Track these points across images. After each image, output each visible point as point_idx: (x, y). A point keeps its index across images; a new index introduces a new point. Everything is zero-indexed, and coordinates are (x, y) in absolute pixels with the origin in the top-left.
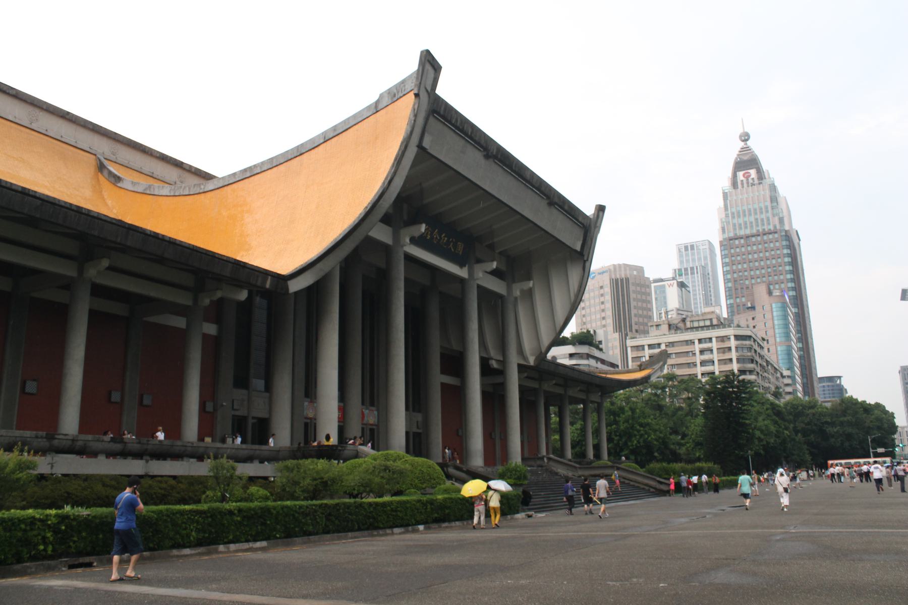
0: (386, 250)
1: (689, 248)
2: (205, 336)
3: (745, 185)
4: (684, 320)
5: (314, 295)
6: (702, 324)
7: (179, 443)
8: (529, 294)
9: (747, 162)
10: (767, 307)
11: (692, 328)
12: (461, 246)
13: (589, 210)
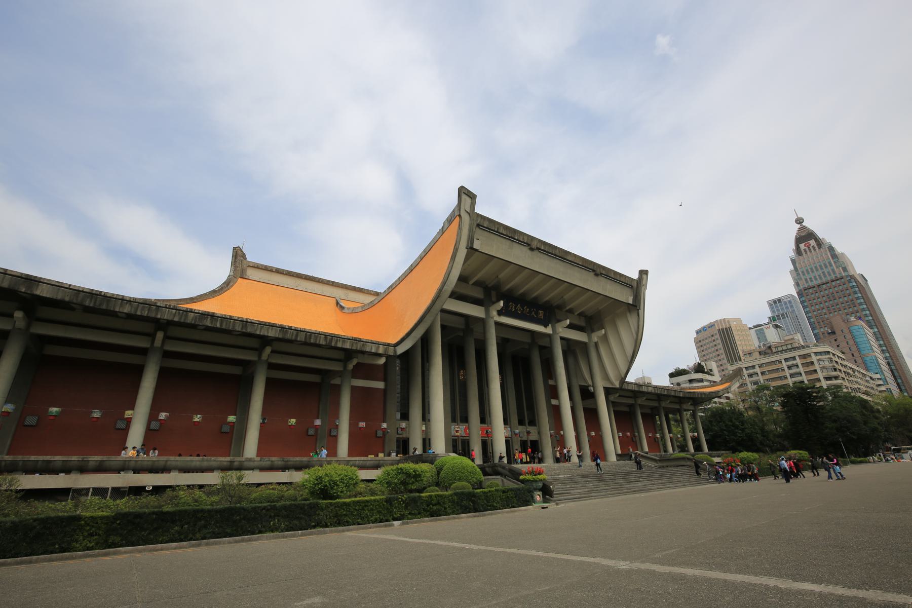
0: (482, 322)
1: (775, 304)
6: (785, 348)
8: (605, 338)
9: (805, 237)
12: (541, 313)
13: (635, 276)
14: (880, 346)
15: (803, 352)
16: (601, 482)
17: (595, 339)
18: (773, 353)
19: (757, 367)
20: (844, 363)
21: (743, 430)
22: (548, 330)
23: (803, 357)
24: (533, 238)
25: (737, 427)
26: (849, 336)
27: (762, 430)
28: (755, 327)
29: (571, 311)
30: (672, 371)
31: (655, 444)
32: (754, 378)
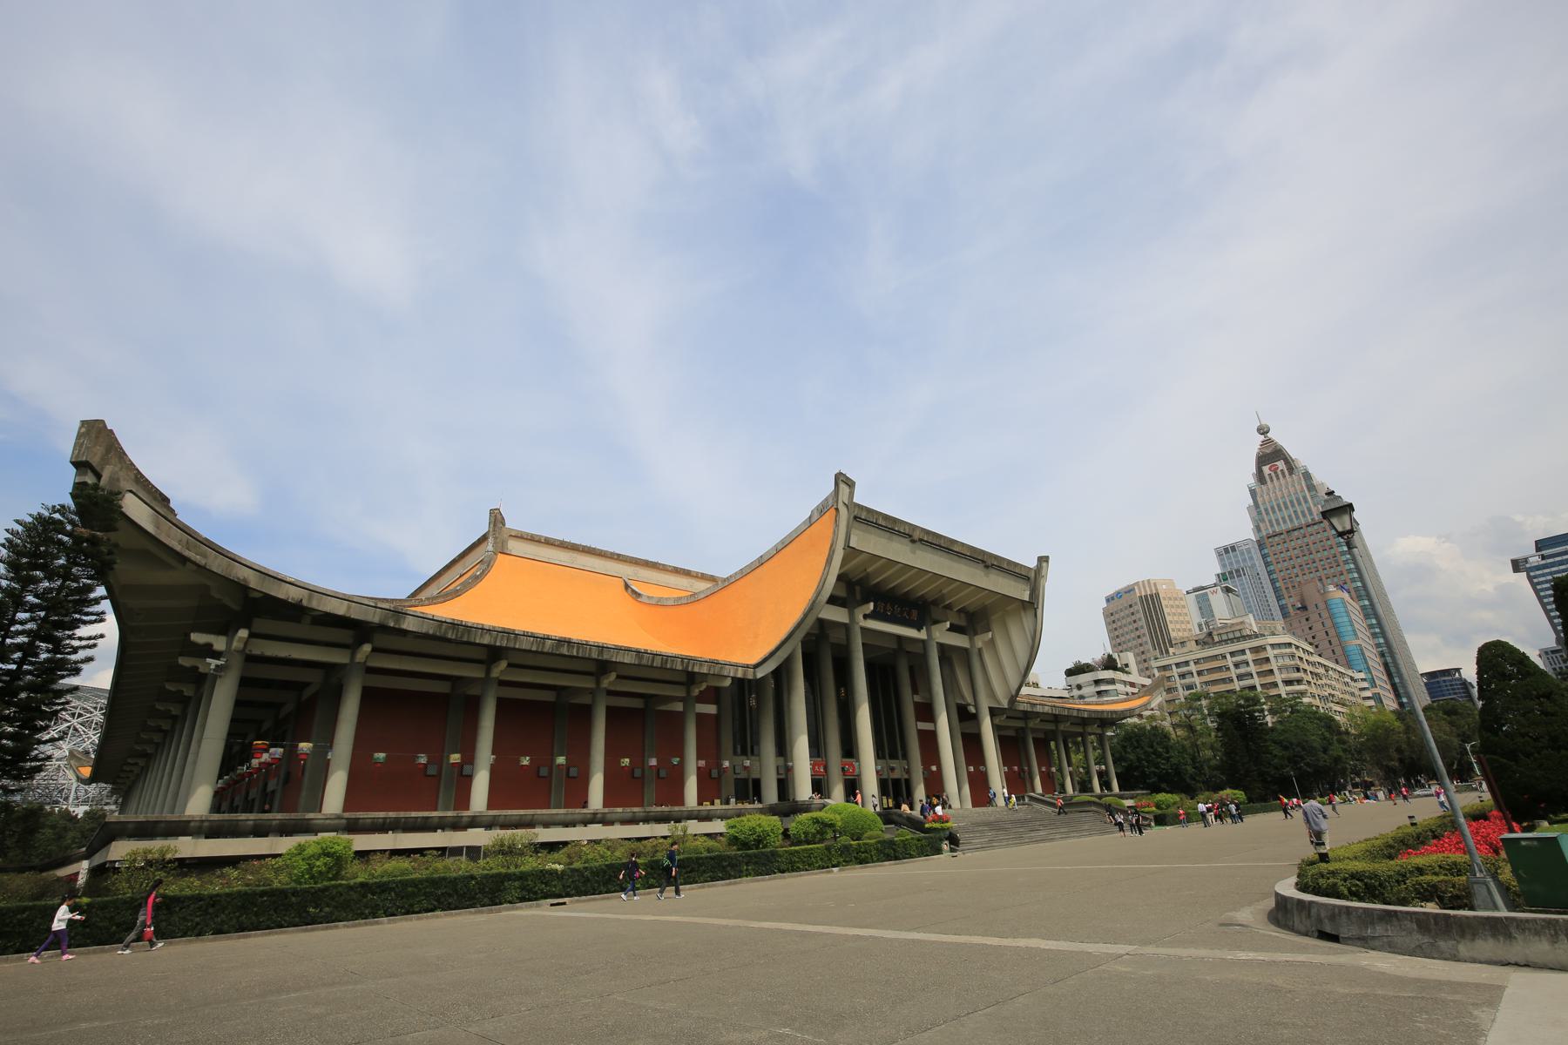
0: (846, 628)
1: (1227, 551)
2: (701, 718)
4: (1210, 634)
5: (781, 675)
7: (466, 813)
8: (992, 642)
9: (1271, 456)
10: (1322, 606)
11: (1220, 642)
12: (915, 613)
13: (1032, 564)
14: (1371, 626)
16: (1000, 830)
17: (979, 644)
18: (1215, 644)
20: (1311, 659)
21: (1168, 759)
22: (922, 635)
23: (1255, 650)
24: (914, 527)
25: (1159, 755)
26: (1325, 614)
27: (1193, 759)
28: (1196, 590)
29: (949, 607)
30: (1070, 666)
31: (1051, 783)
32: (1188, 681)
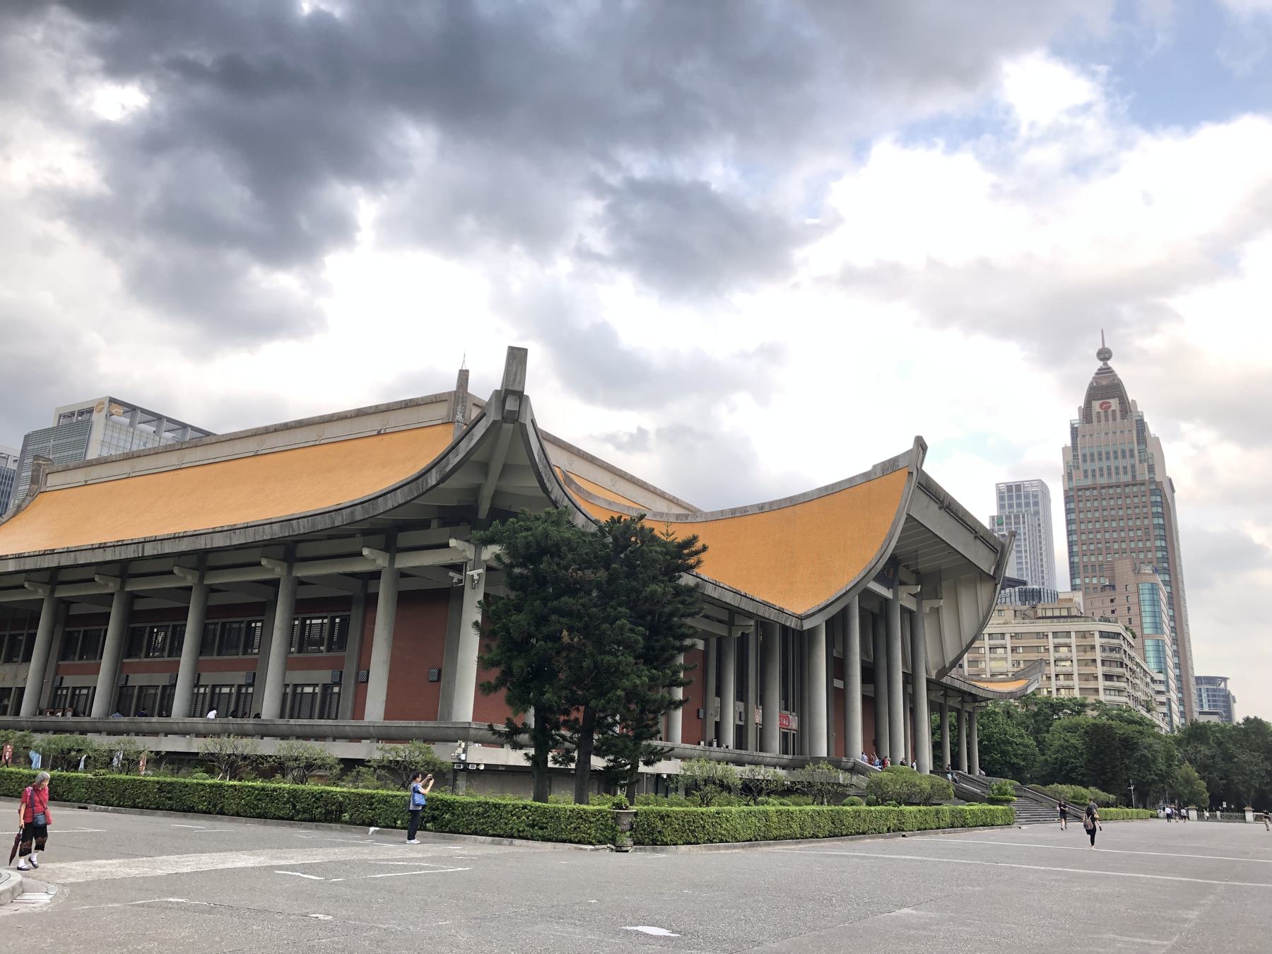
3: (1103, 418)
6: (1057, 613)
8: (937, 611)
10: (1132, 588)
15: (1084, 626)
19: (1008, 637)
20: (1133, 654)
